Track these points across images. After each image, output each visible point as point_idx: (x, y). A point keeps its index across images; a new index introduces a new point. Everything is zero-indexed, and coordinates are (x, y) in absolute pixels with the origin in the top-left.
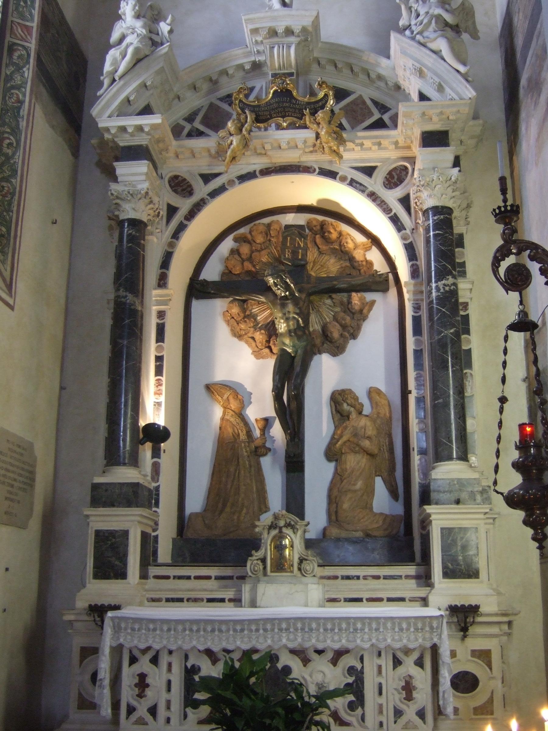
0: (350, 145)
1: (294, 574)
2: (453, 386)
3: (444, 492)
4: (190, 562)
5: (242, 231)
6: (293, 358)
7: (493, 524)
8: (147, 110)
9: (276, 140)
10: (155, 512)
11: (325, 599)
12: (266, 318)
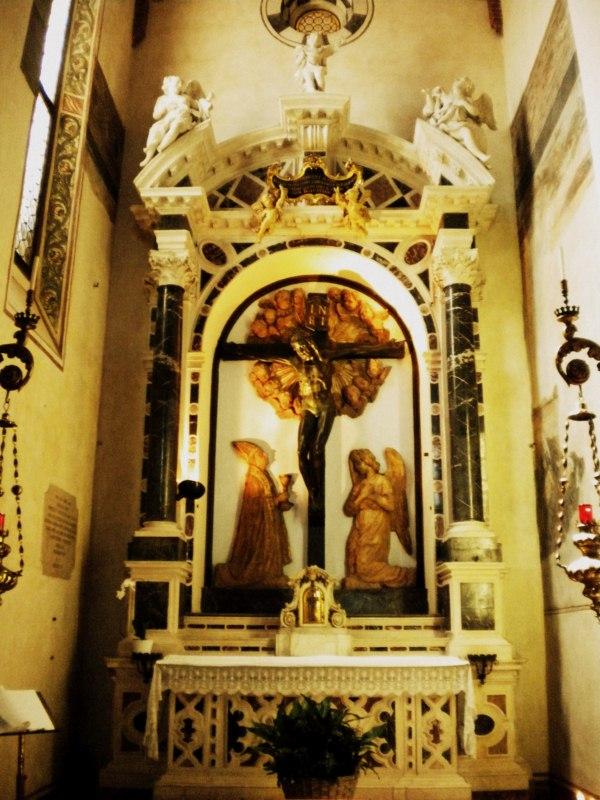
0: (373, 222)
5: (267, 297)
8: (185, 182)
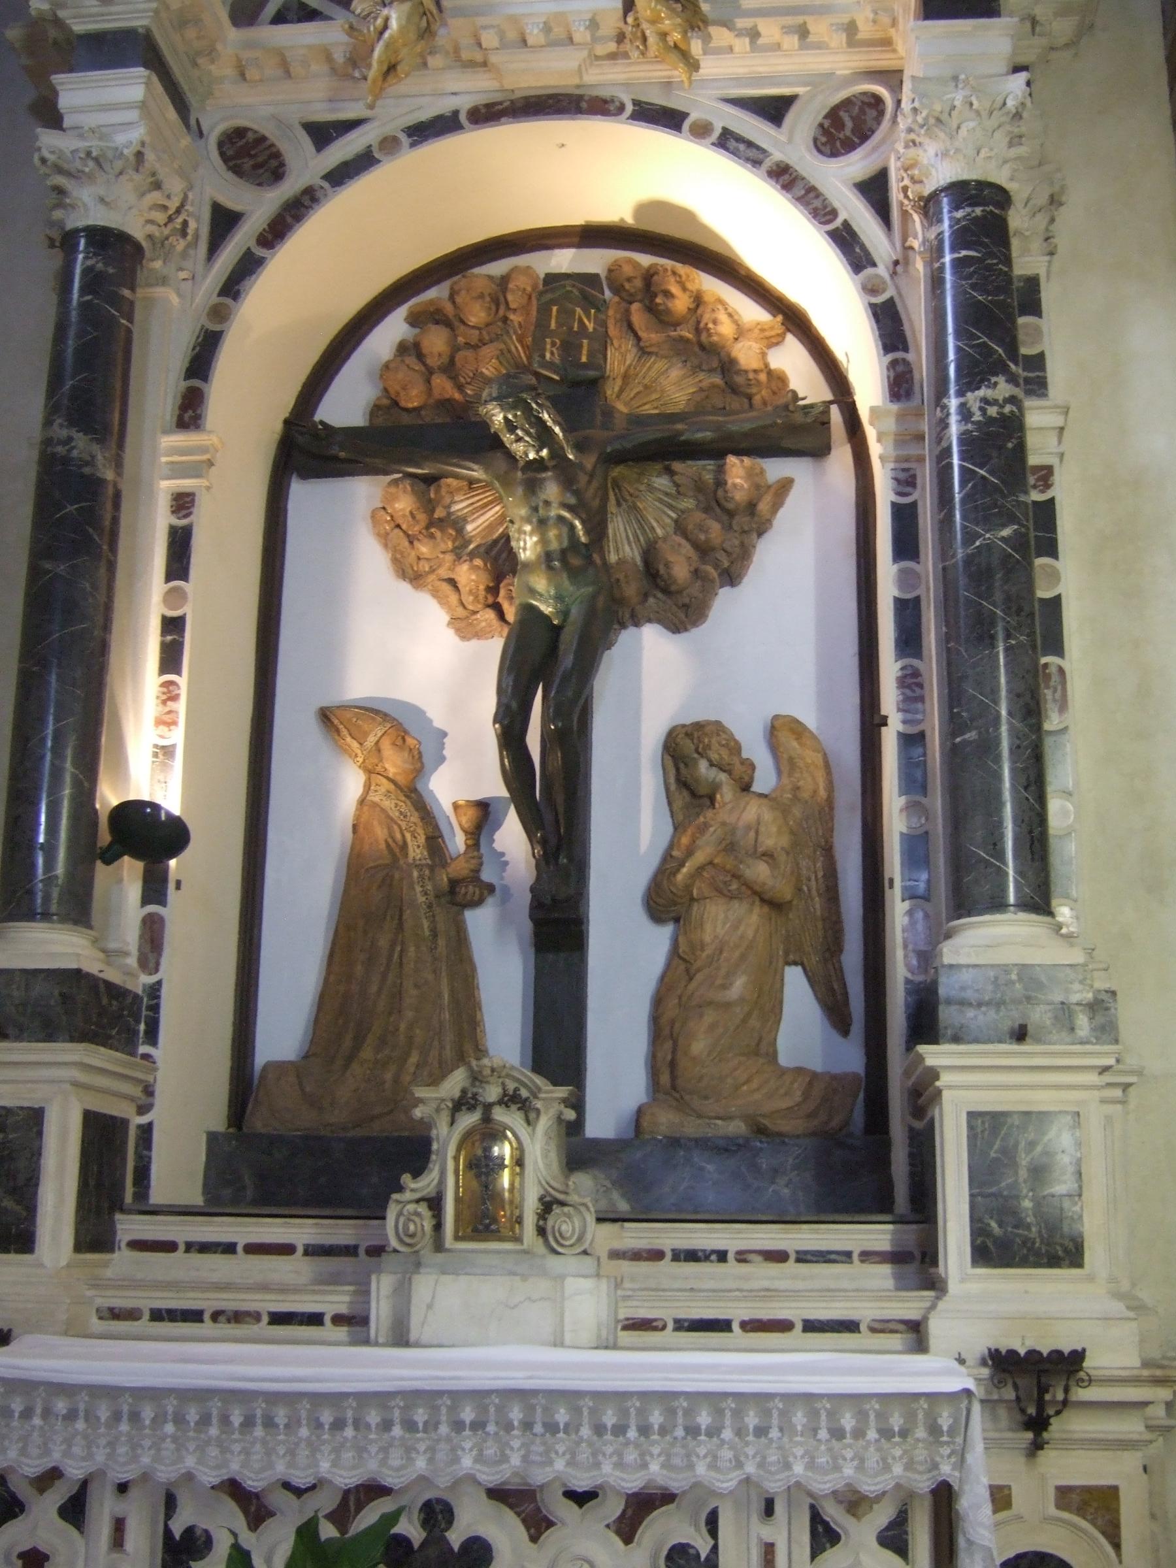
1: (525, 1246)
2: (1009, 691)
3: (980, 1005)
4: (255, 1202)
6: (558, 630)
7: (1123, 1102)
9: (514, 20)
10: (146, 1057)
11: (618, 1321)
12: (491, 527)
